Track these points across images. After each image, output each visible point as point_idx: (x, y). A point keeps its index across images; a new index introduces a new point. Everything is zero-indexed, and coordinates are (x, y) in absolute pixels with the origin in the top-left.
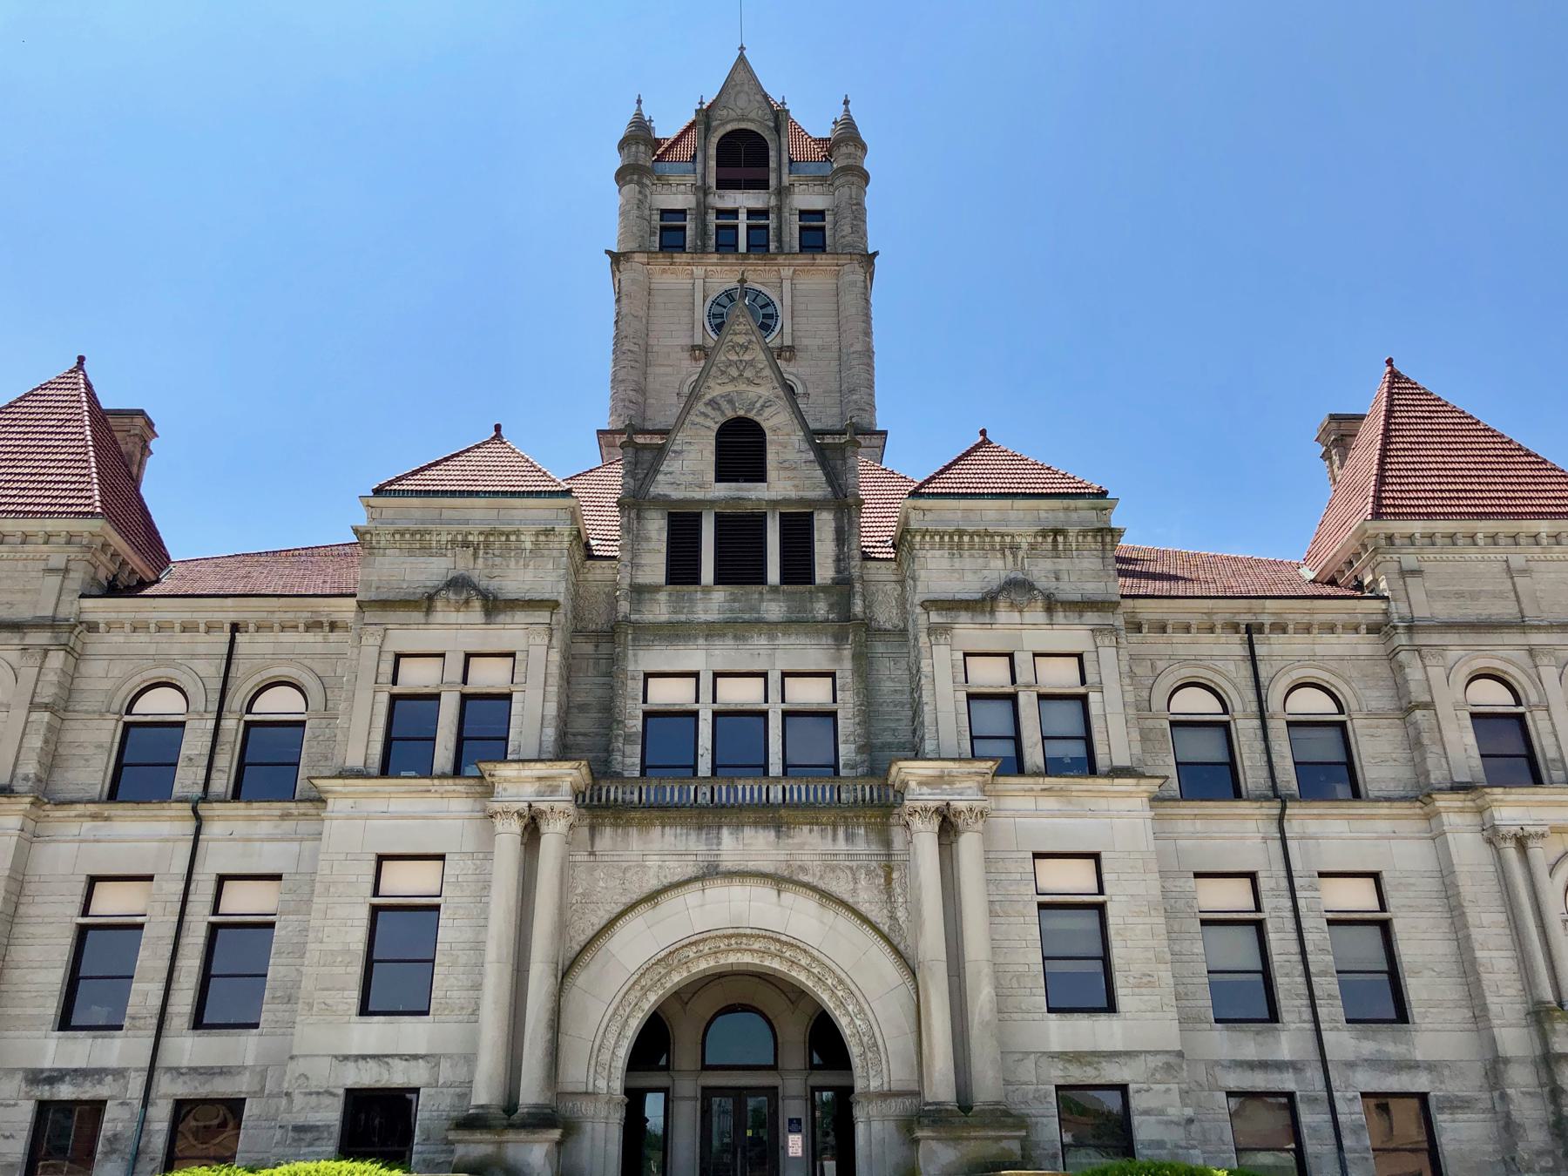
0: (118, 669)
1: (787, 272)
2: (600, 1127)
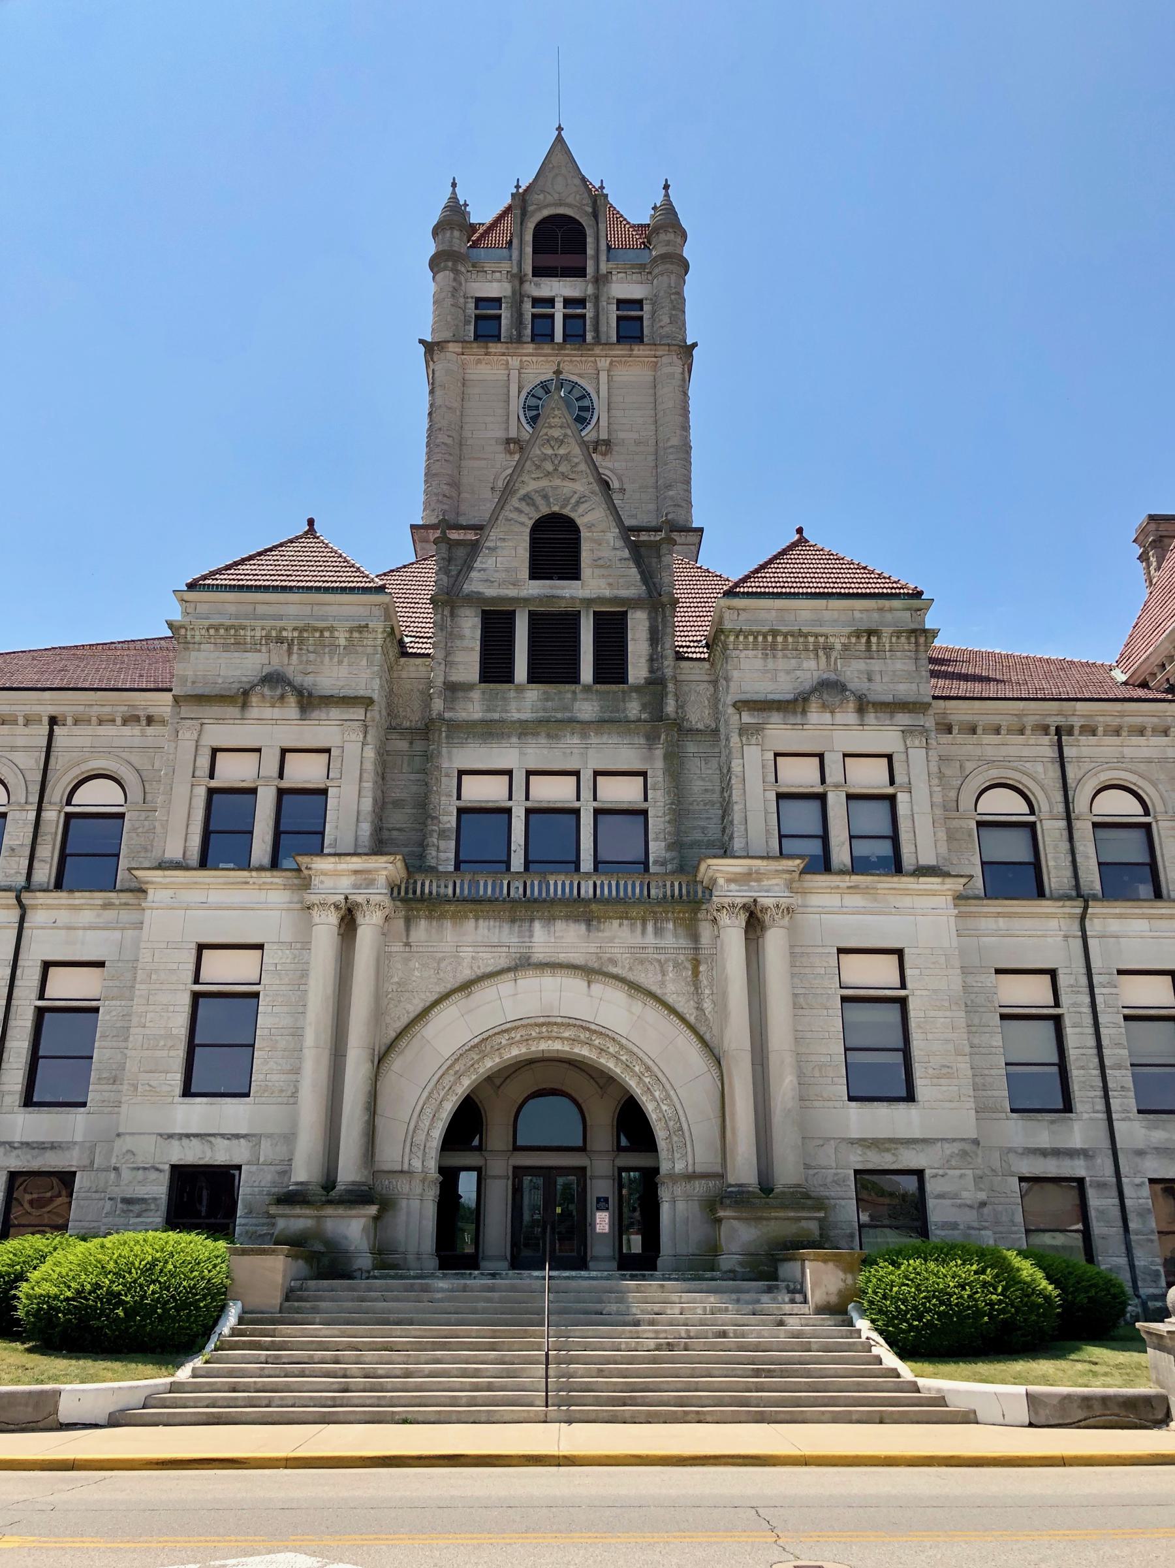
1: (603, 363)
2: (415, 1204)
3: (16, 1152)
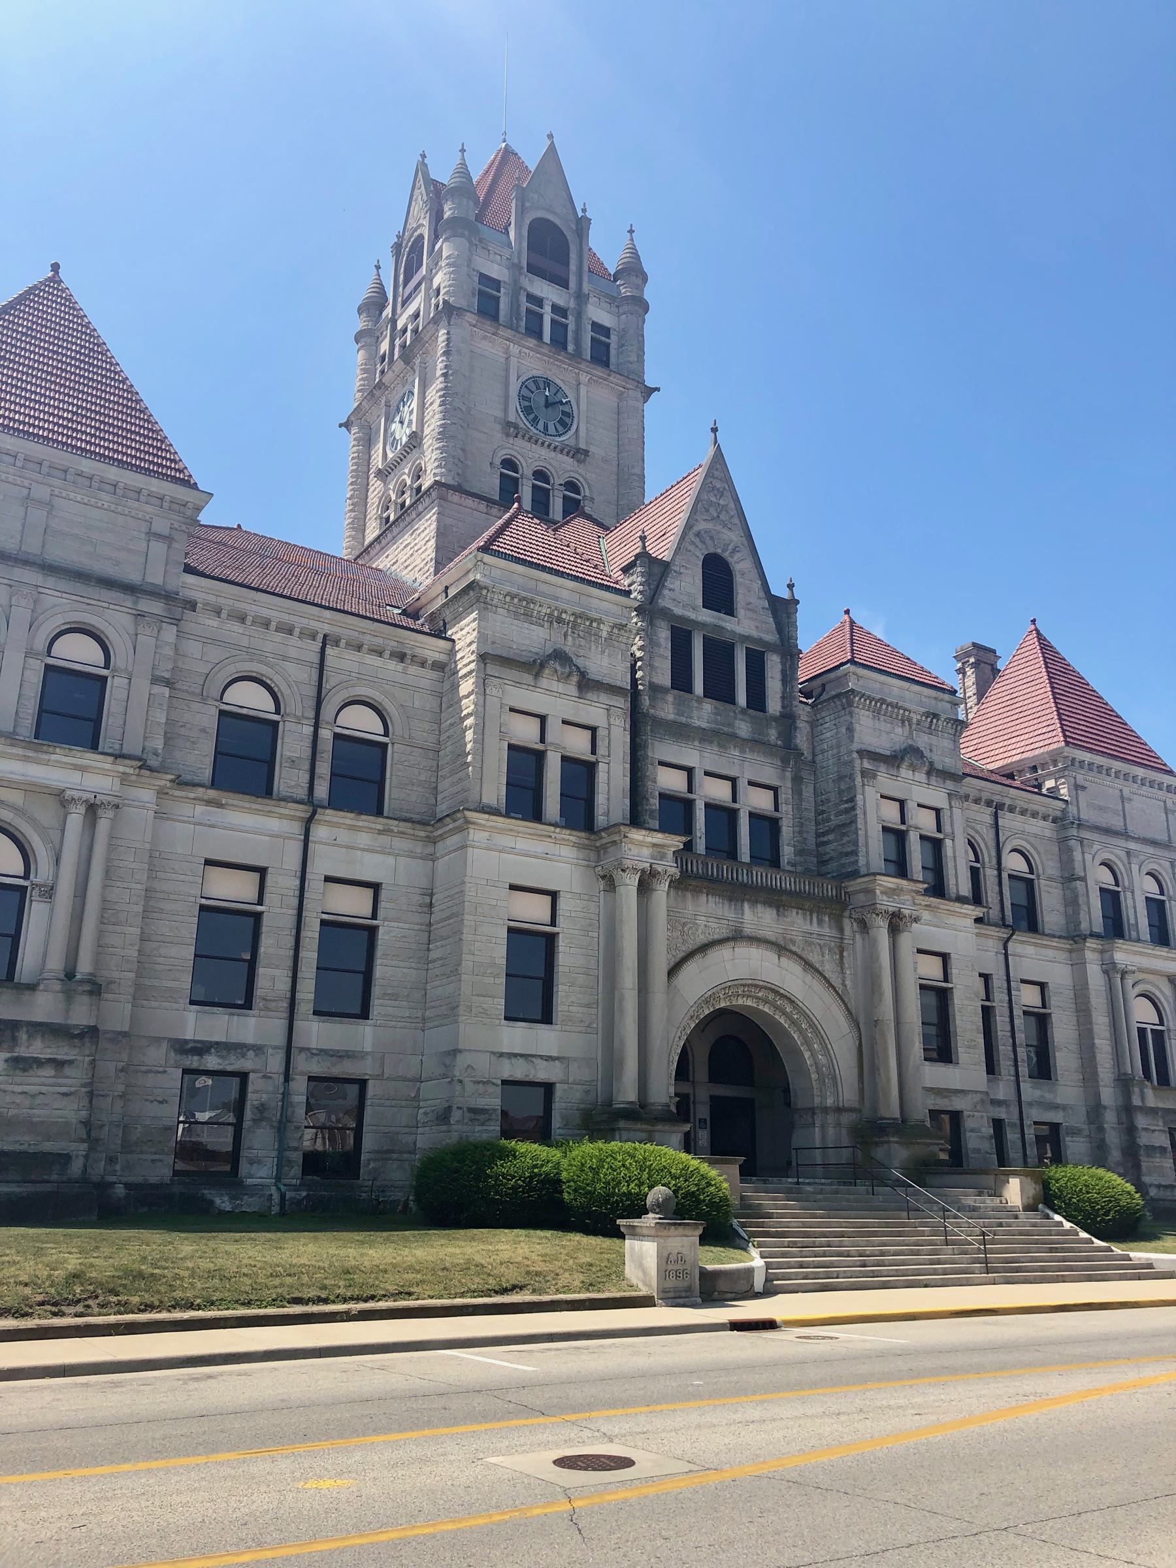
0: (215, 654)
3: (316, 1059)
